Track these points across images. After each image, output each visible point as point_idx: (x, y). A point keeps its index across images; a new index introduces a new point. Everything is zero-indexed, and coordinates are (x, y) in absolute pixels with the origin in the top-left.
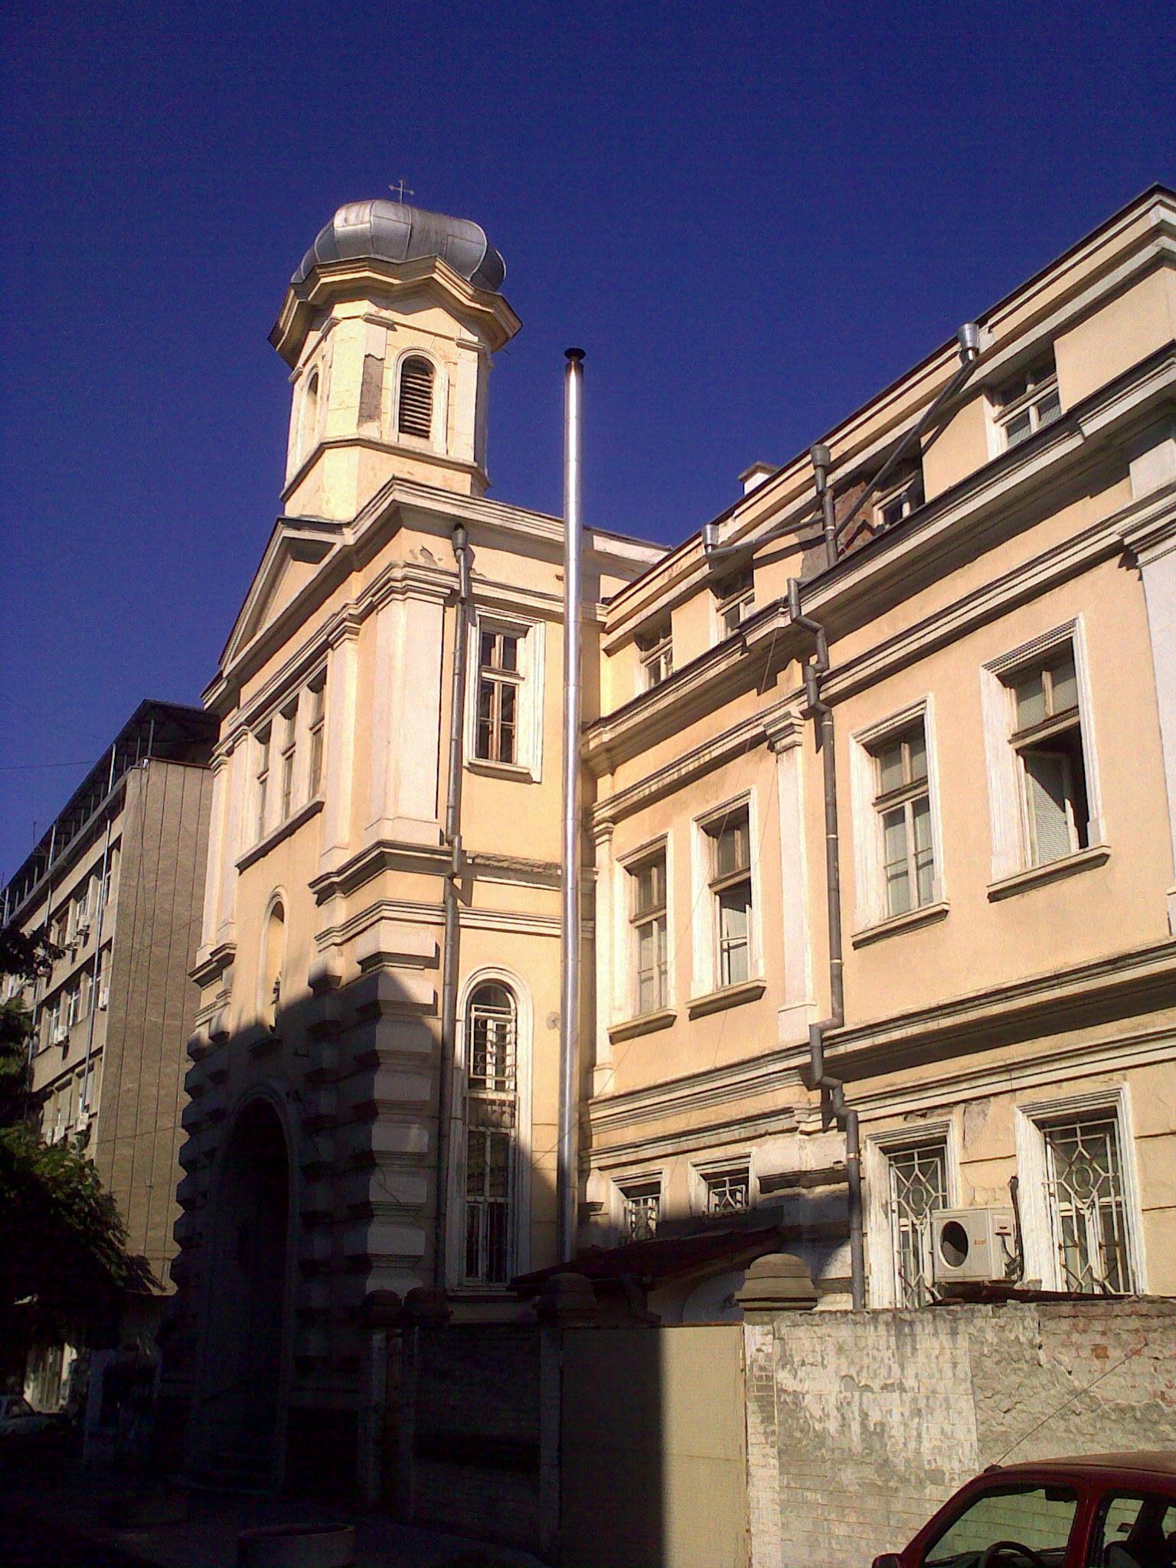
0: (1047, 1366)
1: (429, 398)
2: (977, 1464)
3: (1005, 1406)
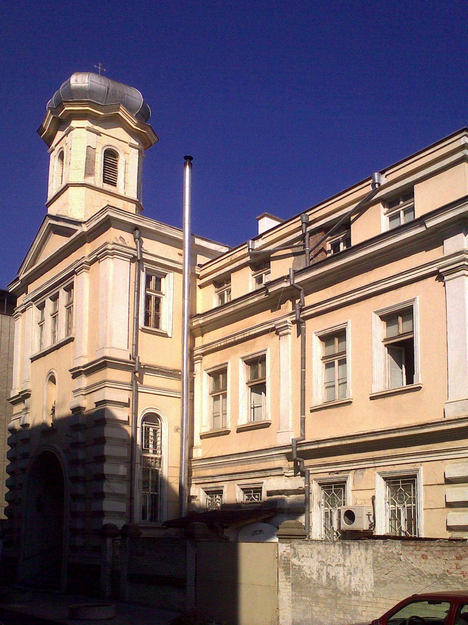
0: (403, 561)
1: (116, 168)
2: (373, 590)
3: (386, 572)
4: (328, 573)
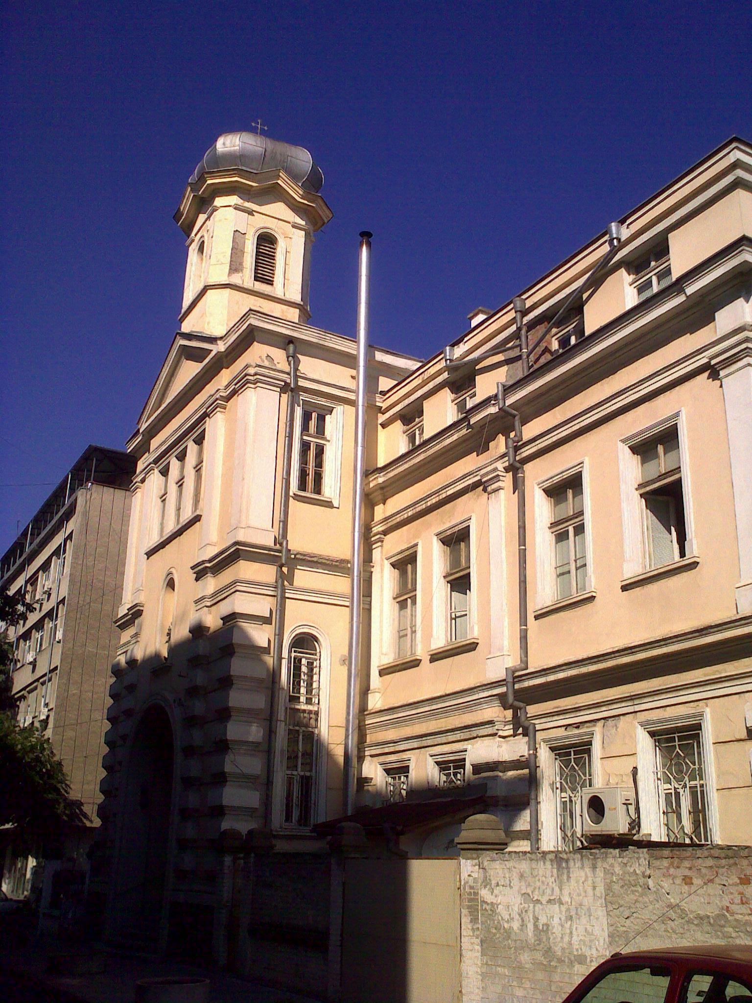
0: (653, 889)
1: (274, 260)
3: (627, 914)
4: (535, 917)
